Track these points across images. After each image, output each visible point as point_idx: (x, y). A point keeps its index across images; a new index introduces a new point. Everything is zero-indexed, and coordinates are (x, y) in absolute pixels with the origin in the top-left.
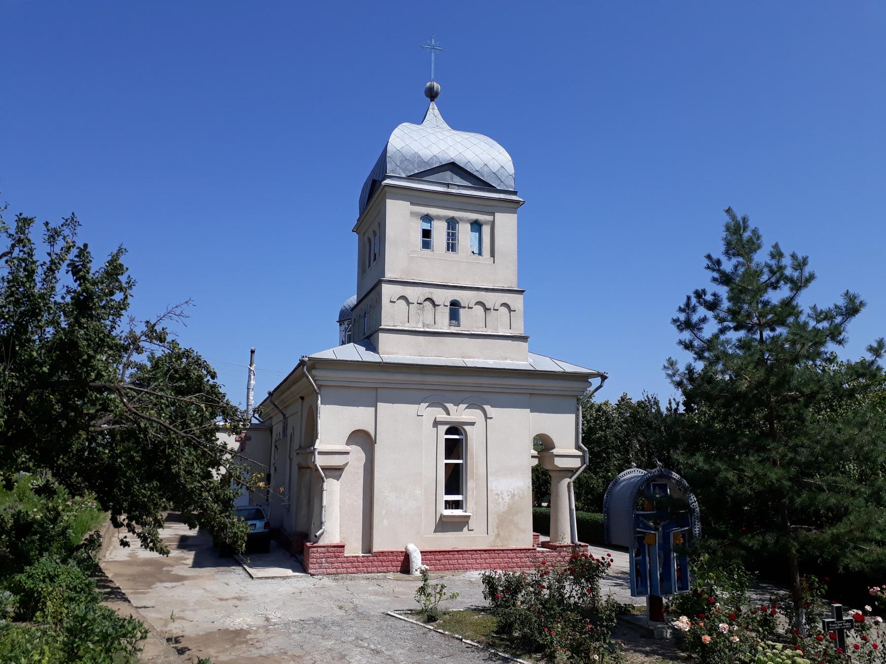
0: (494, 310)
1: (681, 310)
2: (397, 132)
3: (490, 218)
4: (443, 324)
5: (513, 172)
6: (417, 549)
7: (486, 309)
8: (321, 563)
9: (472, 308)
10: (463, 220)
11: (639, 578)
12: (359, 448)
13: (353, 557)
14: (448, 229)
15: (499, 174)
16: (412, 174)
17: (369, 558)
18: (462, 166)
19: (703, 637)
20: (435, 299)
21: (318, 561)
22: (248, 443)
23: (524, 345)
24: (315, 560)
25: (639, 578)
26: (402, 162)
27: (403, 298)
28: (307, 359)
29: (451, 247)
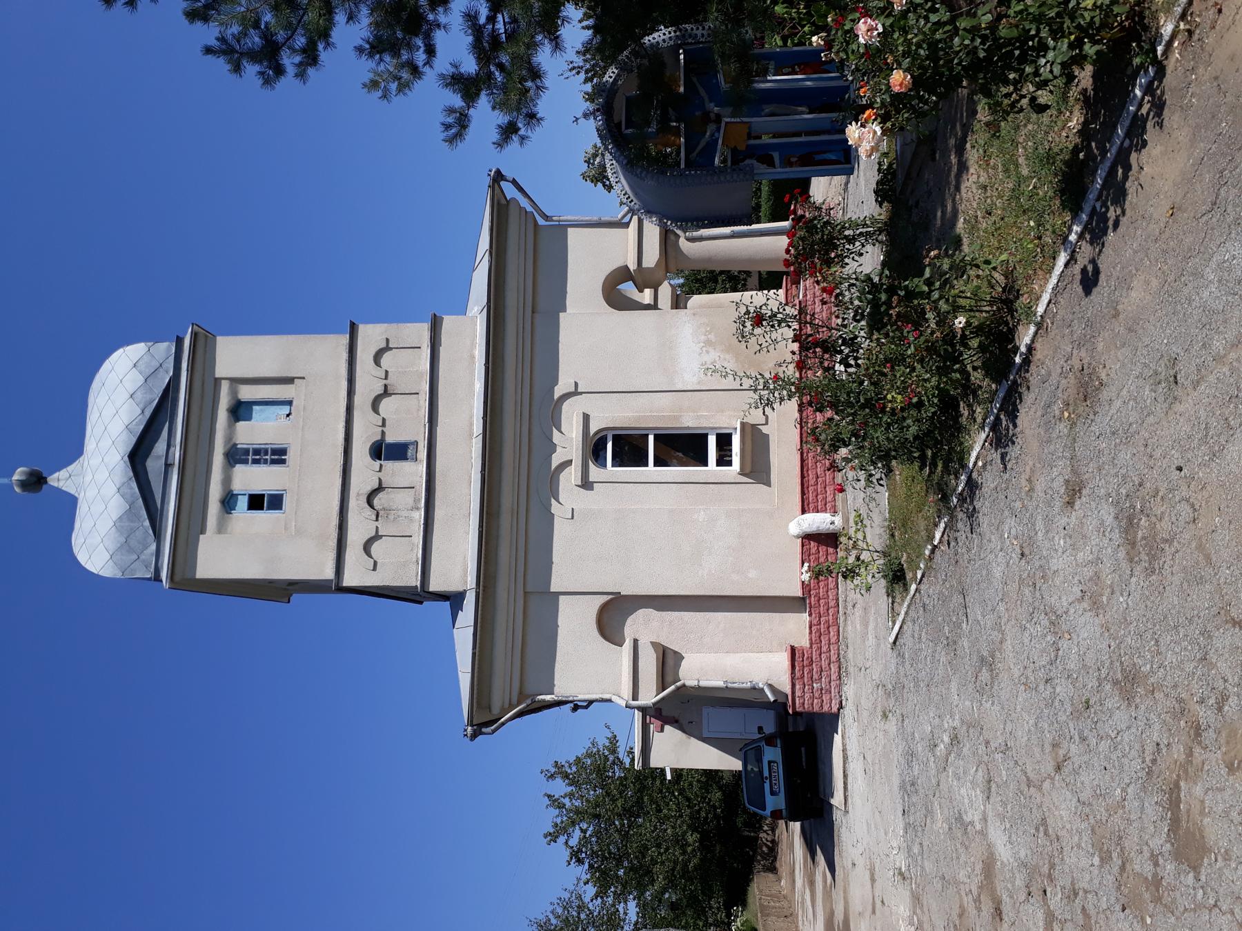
0: (386, 378)
1: (237, 69)
2: (82, 558)
3: (225, 387)
4: (412, 472)
5: (142, 344)
6: (796, 519)
7: (386, 393)
8: (822, 689)
9: (384, 420)
11: (818, 157)
12: (629, 621)
13: (811, 633)
14: (245, 462)
15: (148, 372)
16: (151, 532)
17: (813, 603)
18: (134, 440)
19: (896, 89)
20: (369, 488)
21: (816, 695)
22: (664, 713)
23: (448, 322)
24: (815, 701)
25: (818, 157)
26: (131, 550)
27: (367, 548)
28: (470, 728)
29: (278, 456)
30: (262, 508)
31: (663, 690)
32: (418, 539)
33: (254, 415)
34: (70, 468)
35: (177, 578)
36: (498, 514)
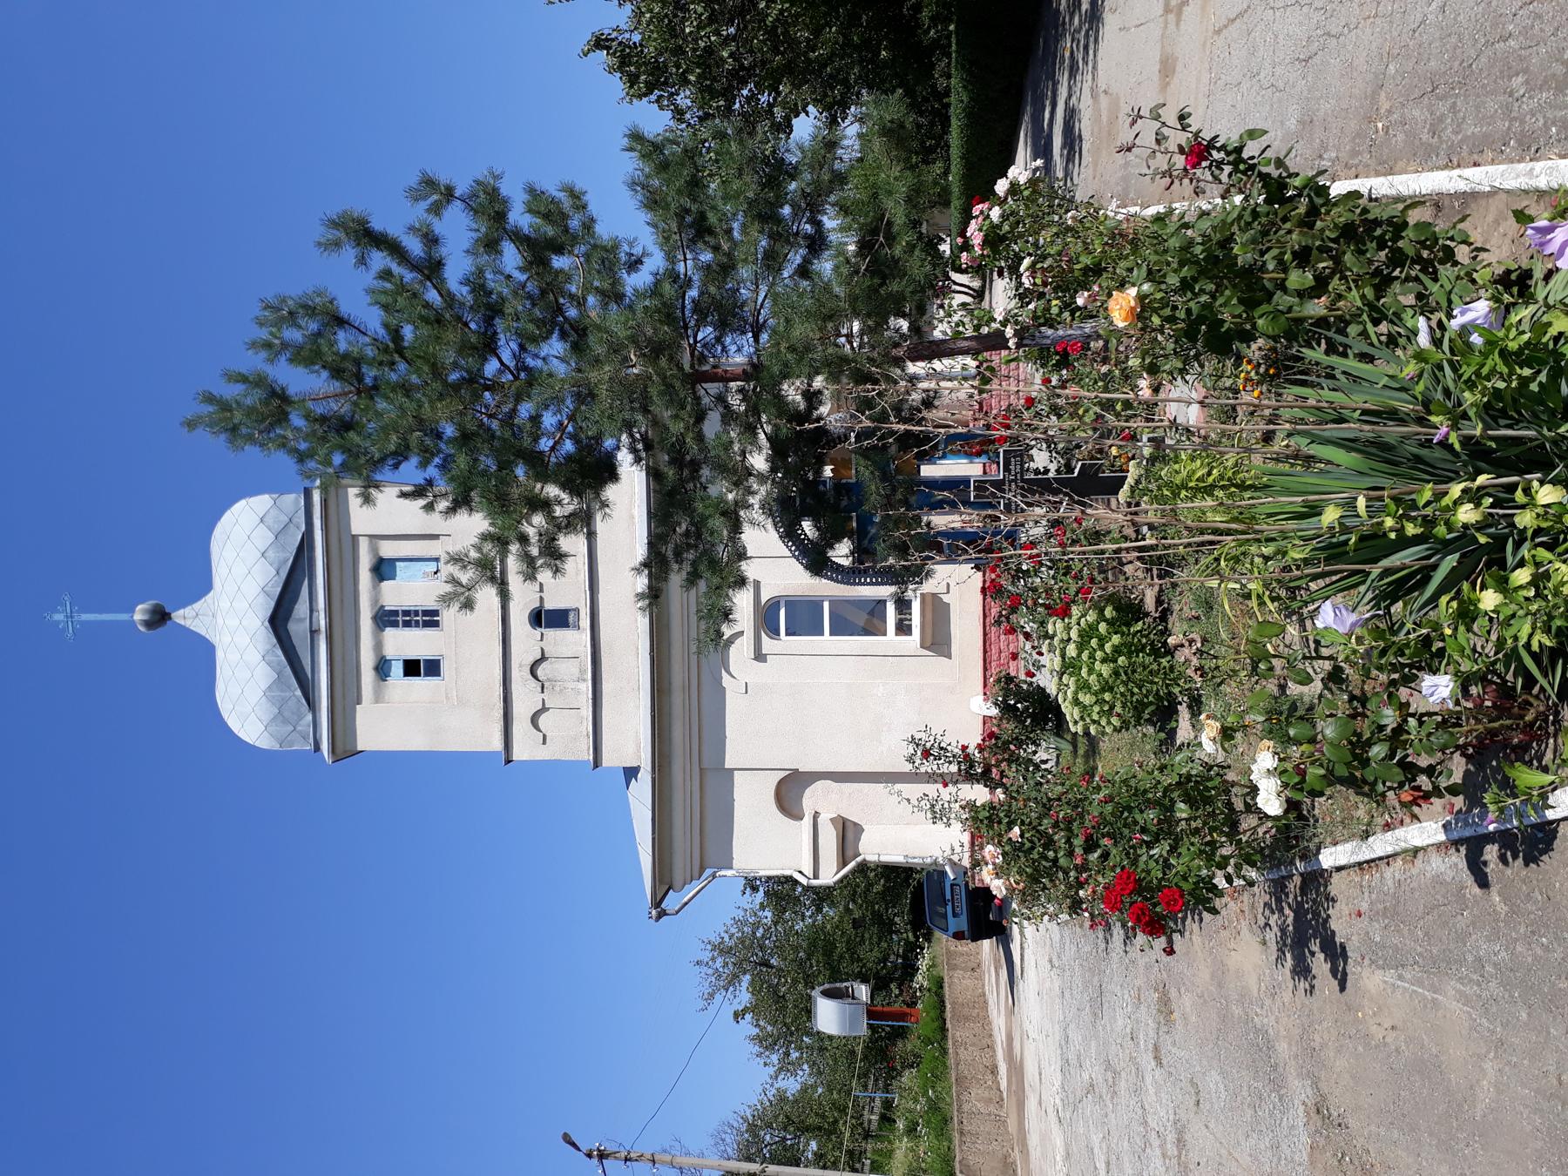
2: (234, 723)
4: (574, 641)
5: (266, 497)
10: (375, 599)
14: (395, 624)
15: (278, 527)
18: (272, 604)
20: (531, 660)
26: (286, 721)
27: (534, 720)
30: (418, 674)
31: (845, 864)
32: (587, 712)
34: (197, 606)
35: (339, 750)
36: (668, 626)
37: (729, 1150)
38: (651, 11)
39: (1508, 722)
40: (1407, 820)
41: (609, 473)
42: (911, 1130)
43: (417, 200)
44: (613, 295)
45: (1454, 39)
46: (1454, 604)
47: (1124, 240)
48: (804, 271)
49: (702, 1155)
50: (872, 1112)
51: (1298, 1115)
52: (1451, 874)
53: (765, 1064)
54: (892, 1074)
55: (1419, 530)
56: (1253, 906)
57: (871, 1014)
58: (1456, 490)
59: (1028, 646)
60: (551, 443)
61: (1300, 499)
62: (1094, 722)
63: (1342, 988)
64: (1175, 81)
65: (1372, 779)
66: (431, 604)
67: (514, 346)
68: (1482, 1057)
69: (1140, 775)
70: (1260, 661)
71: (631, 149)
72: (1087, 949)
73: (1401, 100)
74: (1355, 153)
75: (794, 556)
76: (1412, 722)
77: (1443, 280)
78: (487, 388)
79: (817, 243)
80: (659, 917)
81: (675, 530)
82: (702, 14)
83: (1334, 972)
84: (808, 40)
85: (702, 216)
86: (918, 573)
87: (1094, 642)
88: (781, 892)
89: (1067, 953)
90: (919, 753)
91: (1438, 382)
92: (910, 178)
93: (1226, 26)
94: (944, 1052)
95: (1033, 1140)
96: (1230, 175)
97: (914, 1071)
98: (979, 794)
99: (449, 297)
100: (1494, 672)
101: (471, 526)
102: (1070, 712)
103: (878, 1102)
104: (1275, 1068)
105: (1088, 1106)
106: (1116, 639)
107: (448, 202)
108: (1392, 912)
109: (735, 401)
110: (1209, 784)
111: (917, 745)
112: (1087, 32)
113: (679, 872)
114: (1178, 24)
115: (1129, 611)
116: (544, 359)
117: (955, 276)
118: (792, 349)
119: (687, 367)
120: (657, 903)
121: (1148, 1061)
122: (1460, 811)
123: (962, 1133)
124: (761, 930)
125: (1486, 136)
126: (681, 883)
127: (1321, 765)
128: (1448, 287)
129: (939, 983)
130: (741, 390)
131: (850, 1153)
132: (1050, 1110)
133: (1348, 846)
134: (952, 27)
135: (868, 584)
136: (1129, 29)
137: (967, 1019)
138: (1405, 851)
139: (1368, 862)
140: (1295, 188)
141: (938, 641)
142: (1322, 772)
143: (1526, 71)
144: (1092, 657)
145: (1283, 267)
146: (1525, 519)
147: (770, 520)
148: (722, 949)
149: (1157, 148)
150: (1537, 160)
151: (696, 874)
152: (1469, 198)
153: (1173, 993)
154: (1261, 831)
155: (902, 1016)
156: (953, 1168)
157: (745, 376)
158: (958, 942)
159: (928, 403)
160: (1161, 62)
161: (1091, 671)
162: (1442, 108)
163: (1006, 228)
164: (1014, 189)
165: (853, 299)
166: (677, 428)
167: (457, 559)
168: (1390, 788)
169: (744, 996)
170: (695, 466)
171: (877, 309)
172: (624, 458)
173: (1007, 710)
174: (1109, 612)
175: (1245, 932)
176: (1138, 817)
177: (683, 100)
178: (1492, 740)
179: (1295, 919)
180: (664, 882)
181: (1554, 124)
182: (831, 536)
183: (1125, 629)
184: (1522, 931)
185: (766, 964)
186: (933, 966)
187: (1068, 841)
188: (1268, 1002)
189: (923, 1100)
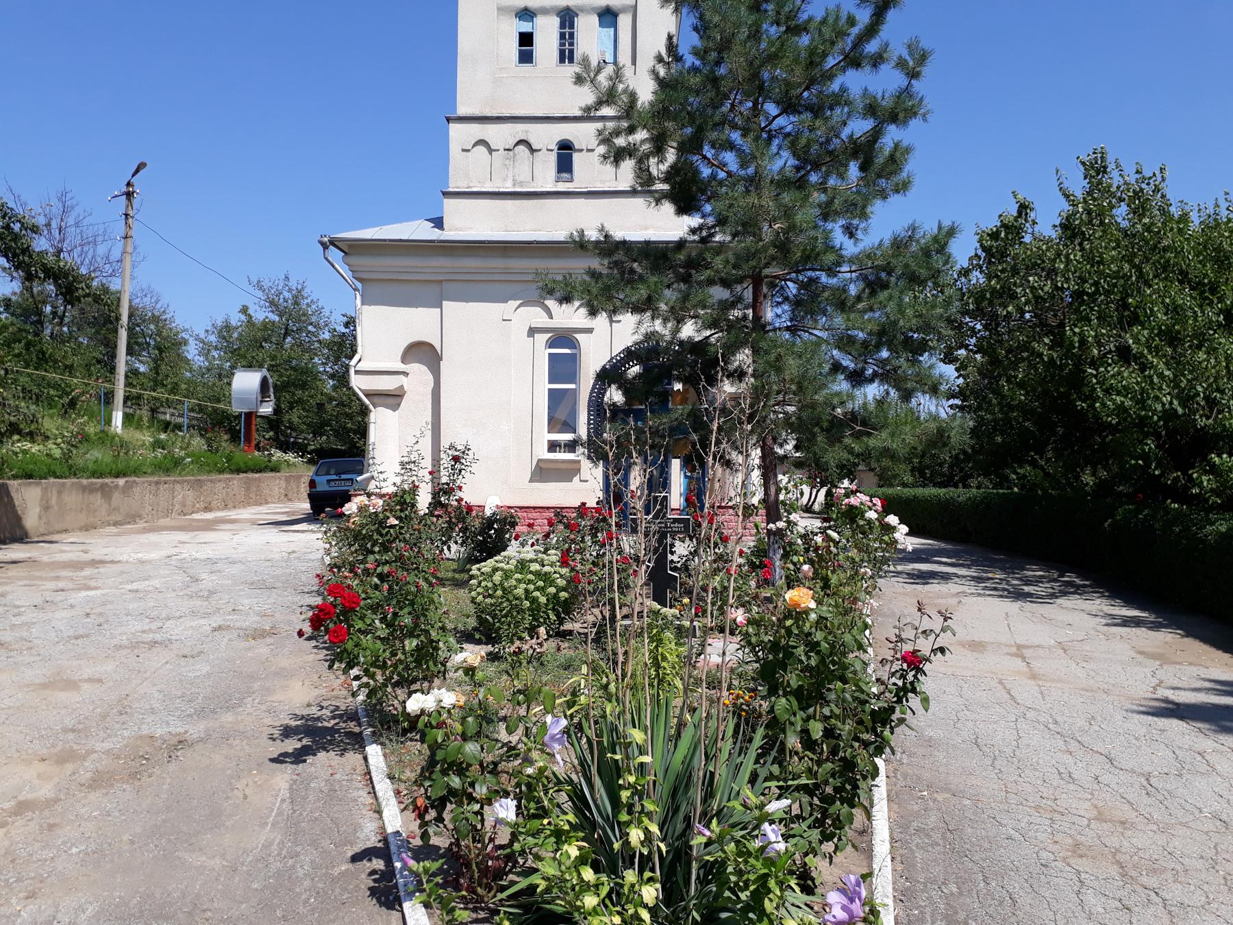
4: (546, 176)
14: (562, 26)
27: (482, 142)
31: (367, 395)
33: (605, 29)
37: (138, 300)
38: (1048, 249)
39: (476, 875)
40: (402, 806)
41: (685, 206)
42: (158, 444)
43: (909, 46)
44: (827, 213)
45: (986, 845)
46: (567, 827)
47: (848, 608)
48: (836, 367)
49: (133, 278)
50: (173, 415)
51: (177, 728)
52: (362, 836)
53: (207, 331)
54: (202, 431)
55: (624, 800)
56: (337, 698)
57: (249, 416)
58: (654, 828)
59: (539, 536)
60: (709, 155)
61: (648, 724)
62: (480, 583)
63: (273, 760)
64: (966, 652)
65: (434, 777)
66: (577, 56)
67: (789, 129)
68: (223, 856)
69: (440, 612)
70: (525, 696)
71: (940, 228)
72: (304, 578)
73: (944, 808)
74: (905, 777)
75: (612, 358)
76: (477, 807)
77: (809, 832)
78: (755, 104)
79: (857, 378)
80: (322, 244)
81: (635, 261)
82: (1042, 290)
83: (285, 755)
84: (1016, 377)
85: (885, 286)
86: (597, 453)
87: (541, 583)
88: (344, 346)
89: (300, 564)
90: (457, 453)
91: (733, 827)
92: (903, 452)
93: (1005, 688)
94: (221, 471)
95: (153, 537)
96: (895, 684)
97: (205, 447)
98: (423, 501)
99: (829, 76)
100: (514, 867)
101: (645, 92)
102: (487, 566)
103: (179, 420)
104: (214, 712)
105: (180, 578)
106: (543, 600)
107: (907, 74)
108: (332, 794)
109: (736, 313)
110: (431, 663)
111: (463, 452)
112: (1007, 590)
113: (361, 261)
114: (1008, 654)
115: (566, 608)
116: (778, 153)
117: (823, 491)
118: (779, 358)
119: (766, 271)
120: (333, 242)
121: (216, 621)
122: (409, 842)
123: (157, 483)
124: (314, 330)
125: (914, 866)
126: (351, 263)
127: (444, 740)
128: (805, 835)
129: (275, 469)
130: (745, 317)
131: (139, 397)
132: (177, 550)
133: (382, 764)
134: (1016, 489)
135: (589, 421)
136: (1006, 619)
137: (248, 489)
138: (379, 805)
139: (371, 779)
140: (882, 732)
141: (543, 472)
142: (440, 740)
143: (961, 894)
144: (530, 582)
145: (826, 719)
146: (630, 876)
147: (642, 338)
148: (297, 298)
149: (920, 631)
150: (895, 901)
151: (357, 275)
152: (869, 853)
153: (269, 640)
154: (396, 702)
155: (248, 439)
156: (130, 475)
157: (757, 318)
158: (307, 484)
159: (728, 464)
160: (980, 642)
161: (519, 581)
162: (937, 836)
163: (861, 523)
164: (890, 529)
165: (813, 406)
166: (718, 262)
167: (618, 75)
168: (426, 790)
169: (261, 314)
170: (686, 279)
171: (804, 428)
172: (694, 221)
173: (489, 522)
174: (564, 595)
175: (317, 692)
176: (406, 610)
177: (977, 278)
178: (462, 864)
179: (326, 728)
180: (351, 249)
181: (921, 912)
182: (627, 387)
183: (551, 606)
184: (319, 885)
185: (286, 334)
186: (289, 465)
187: (387, 562)
188: (263, 707)
189: (182, 453)
